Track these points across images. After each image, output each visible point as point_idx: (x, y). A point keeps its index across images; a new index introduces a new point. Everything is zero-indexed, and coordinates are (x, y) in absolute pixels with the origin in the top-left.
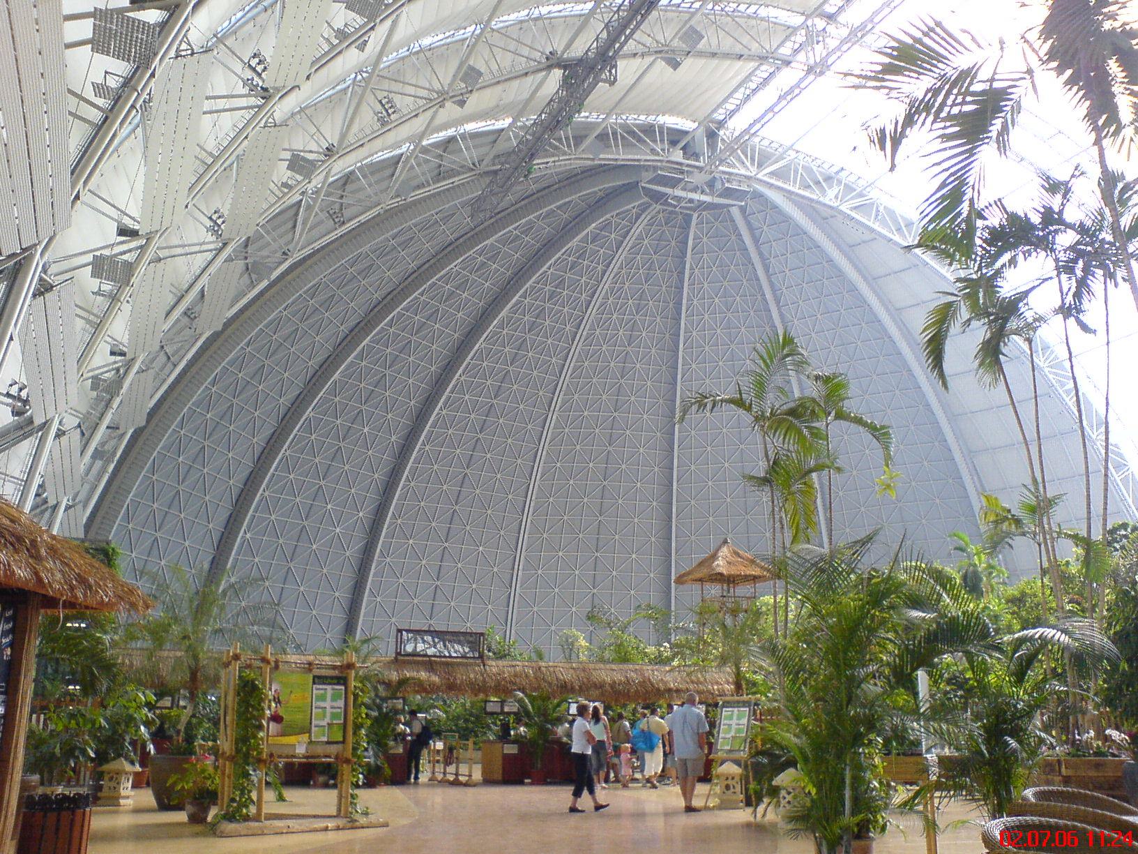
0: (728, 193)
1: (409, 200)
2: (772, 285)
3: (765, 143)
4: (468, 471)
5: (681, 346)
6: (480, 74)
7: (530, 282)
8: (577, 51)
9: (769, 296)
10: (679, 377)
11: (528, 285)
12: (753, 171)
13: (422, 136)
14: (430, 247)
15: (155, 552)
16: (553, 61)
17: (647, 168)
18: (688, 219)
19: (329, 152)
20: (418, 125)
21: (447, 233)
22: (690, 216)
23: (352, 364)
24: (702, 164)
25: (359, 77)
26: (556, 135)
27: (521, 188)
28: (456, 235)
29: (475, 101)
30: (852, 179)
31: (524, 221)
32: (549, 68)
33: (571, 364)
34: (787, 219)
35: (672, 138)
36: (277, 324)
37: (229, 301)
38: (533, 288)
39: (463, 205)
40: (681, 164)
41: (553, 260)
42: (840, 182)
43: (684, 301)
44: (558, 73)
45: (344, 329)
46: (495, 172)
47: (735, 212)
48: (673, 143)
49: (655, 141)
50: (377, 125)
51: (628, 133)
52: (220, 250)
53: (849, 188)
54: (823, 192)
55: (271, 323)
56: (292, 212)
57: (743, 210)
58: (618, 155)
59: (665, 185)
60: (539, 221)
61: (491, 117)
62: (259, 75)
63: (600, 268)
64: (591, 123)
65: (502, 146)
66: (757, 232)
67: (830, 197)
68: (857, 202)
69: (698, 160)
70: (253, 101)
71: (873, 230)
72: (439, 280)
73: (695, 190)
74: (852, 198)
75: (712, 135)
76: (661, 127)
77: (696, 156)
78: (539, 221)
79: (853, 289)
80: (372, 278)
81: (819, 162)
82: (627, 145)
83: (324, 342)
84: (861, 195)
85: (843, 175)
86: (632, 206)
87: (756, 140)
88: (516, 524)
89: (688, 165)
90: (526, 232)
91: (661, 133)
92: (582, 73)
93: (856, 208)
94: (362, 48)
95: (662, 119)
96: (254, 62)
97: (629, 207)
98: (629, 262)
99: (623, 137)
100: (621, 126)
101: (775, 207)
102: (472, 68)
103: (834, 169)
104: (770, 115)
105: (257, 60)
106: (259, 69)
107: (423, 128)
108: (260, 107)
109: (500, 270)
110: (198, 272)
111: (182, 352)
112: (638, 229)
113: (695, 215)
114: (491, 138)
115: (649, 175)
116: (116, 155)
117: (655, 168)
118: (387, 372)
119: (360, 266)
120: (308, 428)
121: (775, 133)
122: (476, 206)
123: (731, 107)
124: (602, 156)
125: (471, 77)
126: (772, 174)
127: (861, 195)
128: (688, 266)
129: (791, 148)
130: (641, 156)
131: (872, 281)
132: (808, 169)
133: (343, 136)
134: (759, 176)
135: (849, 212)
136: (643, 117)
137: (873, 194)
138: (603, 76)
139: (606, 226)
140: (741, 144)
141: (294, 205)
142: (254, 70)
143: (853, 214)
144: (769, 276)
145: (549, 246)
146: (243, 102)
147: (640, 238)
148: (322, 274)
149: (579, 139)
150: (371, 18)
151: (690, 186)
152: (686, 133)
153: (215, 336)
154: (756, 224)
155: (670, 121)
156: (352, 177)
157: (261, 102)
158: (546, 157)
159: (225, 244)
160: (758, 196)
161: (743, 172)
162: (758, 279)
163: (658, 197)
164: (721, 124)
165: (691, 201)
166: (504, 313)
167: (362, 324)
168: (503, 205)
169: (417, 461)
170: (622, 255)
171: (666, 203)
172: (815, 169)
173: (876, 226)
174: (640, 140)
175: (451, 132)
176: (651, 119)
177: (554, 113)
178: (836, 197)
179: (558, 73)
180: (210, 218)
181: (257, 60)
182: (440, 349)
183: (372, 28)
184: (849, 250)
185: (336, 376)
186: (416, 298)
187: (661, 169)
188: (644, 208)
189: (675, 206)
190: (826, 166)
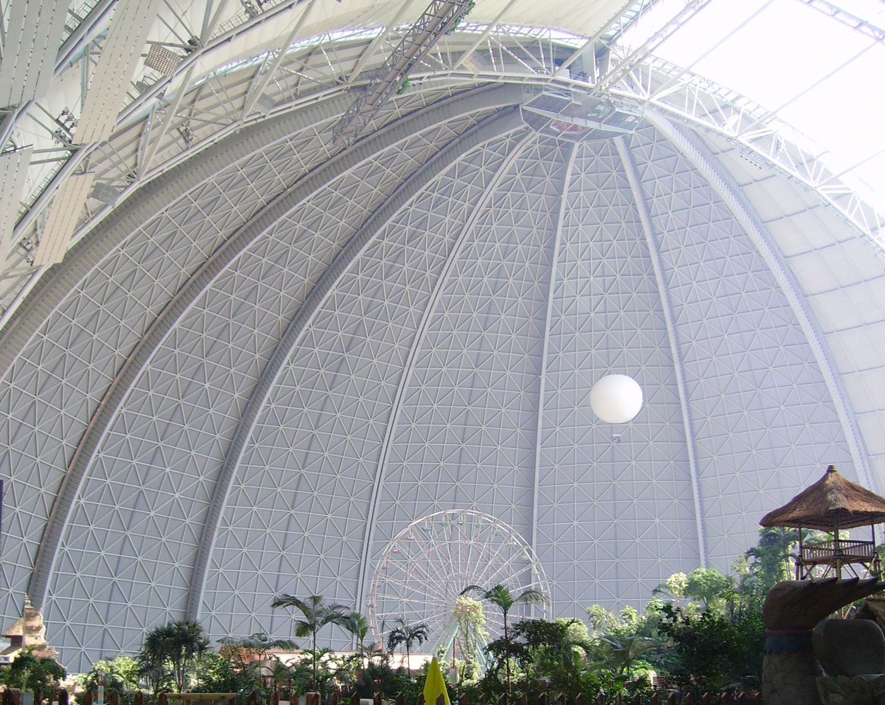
2: (652, 228)
3: (658, 64)
5: (551, 294)
7: (389, 221)
9: (649, 240)
10: (548, 329)
11: (386, 225)
12: (644, 96)
14: (280, 179)
15: (92, 324)
17: (528, 88)
18: (567, 148)
19: (193, 46)
22: (569, 146)
23: (193, 312)
24: (589, 85)
26: (432, 50)
27: (395, 106)
28: (310, 166)
30: (751, 107)
33: (430, 314)
34: (675, 152)
35: (559, 57)
37: (75, 221)
40: (567, 84)
41: (414, 197)
42: (737, 111)
43: (557, 244)
45: (185, 271)
46: (364, 88)
47: (618, 140)
48: (559, 62)
49: (539, 59)
50: (245, 18)
51: (512, 49)
52: (69, 159)
53: (747, 119)
54: (720, 121)
57: (627, 140)
58: (501, 73)
59: (548, 109)
60: (403, 152)
62: (68, 130)
65: (373, 60)
66: (640, 168)
67: (730, 126)
71: (773, 166)
75: (601, 53)
76: (546, 45)
77: (583, 76)
78: (403, 152)
79: (742, 234)
81: (716, 87)
82: (508, 60)
85: (740, 104)
86: (504, 135)
87: (648, 60)
89: (576, 86)
91: (546, 51)
93: (754, 140)
95: (545, 35)
96: (62, 119)
97: (502, 135)
98: (499, 199)
99: (505, 55)
101: (663, 139)
103: (731, 97)
104: (672, 28)
105: (65, 117)
106: (68, 125)
109: (355, 208)
111: (18, 289)
112: (512, 160)
113: (577, 145)
114: (357, 51)
117: (538, 89)
118: (231, 321)
121: (672, 54)
122: (338, 129)
123: (624, 20)
127: (758, 127)
128: (563, 205)
129: (687, 71)
131: (761, 224)
132: (704, 96)
133: (206, 30)
134: (653, 100)
135: (748, 144)
136: (525, 31)
137: (772, 127)
140: (633, 67)
142: (63, 125)
143: (753, 147)
145: (411, 181)
146: (54, 155)
147: (512, 172)
148: (163, 208)
152: (572, 51)
153: (55, 270)
154: (639, 158)
155: (557, 37)
158: (420, 71)
159: (74, 152)
160: (646, 126)
161: (632, 94)
162: (638, 221)
163: (536, 122)
164: (611, 40)
165: (575, 128)
166: (359, 256)
168: (367, 130)
170: (492, 191)
171: (548, 131)
172: (713, 97)
173: (776, 161)
174: (526, 59)
175: (314, 41)
176: (535, 33)
177: (440, 14)
178: (735, 128)
180: (57, 121)
181: (65, 117)
182: (288, 297)
184: (738, 189)
185: (176, 325)
187: (546, 90)
188: (518, 138)
190: (723, 92)
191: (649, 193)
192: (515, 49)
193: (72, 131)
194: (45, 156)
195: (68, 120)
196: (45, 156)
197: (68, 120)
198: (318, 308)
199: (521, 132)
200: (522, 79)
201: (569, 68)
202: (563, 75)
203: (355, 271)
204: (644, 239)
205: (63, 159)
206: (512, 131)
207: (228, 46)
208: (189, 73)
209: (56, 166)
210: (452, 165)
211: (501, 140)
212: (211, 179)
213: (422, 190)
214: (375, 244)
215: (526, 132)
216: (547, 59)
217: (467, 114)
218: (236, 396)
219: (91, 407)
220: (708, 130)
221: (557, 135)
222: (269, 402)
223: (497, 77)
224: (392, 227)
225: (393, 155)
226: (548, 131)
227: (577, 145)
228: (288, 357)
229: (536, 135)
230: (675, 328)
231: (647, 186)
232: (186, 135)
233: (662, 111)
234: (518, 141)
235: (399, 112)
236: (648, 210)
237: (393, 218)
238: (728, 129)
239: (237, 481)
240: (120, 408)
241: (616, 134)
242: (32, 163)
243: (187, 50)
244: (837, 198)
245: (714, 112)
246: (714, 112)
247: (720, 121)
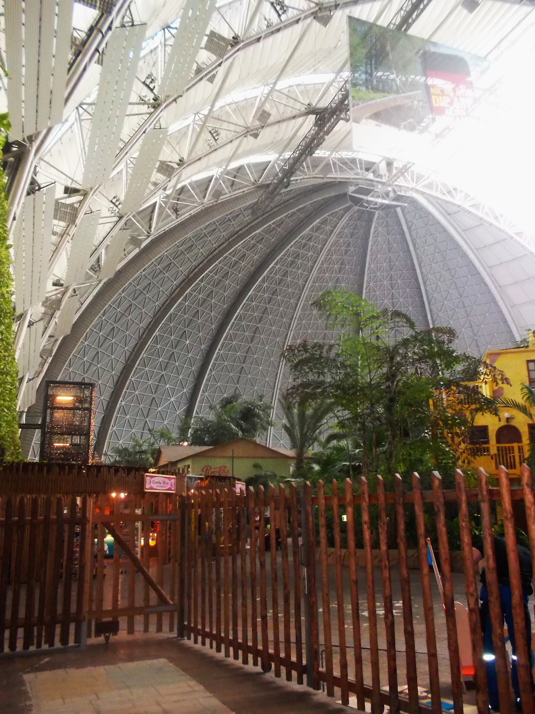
0: (398, 198)
1: (219, 202)
4: (244, 365)
6: (269, 115)
8: (324, 104)
11: (278, 258)
13: (230, 160)
16: (311, 111)
20: (228, 150)
21: (235, 225)
25: (197, 118)
29: (266, 135)
31: (279, 218)
32: (307, 113)
36: (139, 281)
38: (191, 294)
39: (246, 209)
44: (312, 118)
47: (399, 210)
48: (367, 170)
55: (135, 279)
56: (150, 210)
57: (403, 209)
58: (335, 175)
61: (265, 155)
62: (117, 206)
63: (320, 246)
64: (320, 157)
66: (410, 224)
67: (458, 200)
68: (472, 203)
69: (382, 178)
70: (144, 109)
72: (229, 254)
73: (378, 197)
74: (470, 200)
76: (360, 161)
80: (192, 253)
82: (341, 170)
83: (166, 290)
84: (473, 199)
86: (338, 209)
88: (270, 394)
90: (279, 226)
92: (325, 118)
93: (471, 206)
94: (211, 80)
96: (114, 201)
99: (340, 167)
100: (339, 159)
102: (264, 112)
105: (150, 80)
106: (117, 203)
107: (231, 155)
108: (151, 114)
110: (101, 239)
113: (377, 212)
115: (352, 189)
116: (59, 142)
119: (185, 246)
120: (156, 342)
122: (254, 209)
124: (328, 176)
125: (263, 116)
126: (424, 186)
130: (349, 175)
134: (419, 188)
138: (342, 116)
139: (324, 222)
141: (151, 205)
142: (114, 204)
143: (471, 209)
144: (415, 250)
145: (291, 234)
146: (109, 220)
147: (344, 228)
148: (165, 250)
149: (315, 167)
150: (221, 56)
151: (376, 194)
154: (409, 219)
156: (185, 189)
157: (152, 110)
160: (413, 202)
163: (357, 201)
165: (376, 204)
167: (186, 281)
169: (216, 360)
171: (362, 206)
179: (312, 118)
180: (111, 201)
183: (220, 65)
186: (216, 265)
189: (367, 207)
191: (414, 236)
192: (345, 163)
193: (120, 206)
194: (105, 220)
195: (117, 201)
196: (105, 220)
197: (117, 201)
198: (244, 301)
199: (347, 207)
200: (349, 179)
201: (373, 172)
202: (370, 176)
203: (263, 281)
204: (412, 260)
205: (148, 113)
206: (342, 207)
207: (199, 163)
208: (180, 177)
209: (111, 225)
210: (312, 225)
211: (337, 212)
212: (190, 235)
213: (297, 239)
214: (273, 267)
215: (349, 208)
216: (361, 168)
217: (318, 198)
218: (203, 347)
219: (116, 378)
220: (447, 202)
221: (367, 207)
222: (219, 350)
223: (336, 178)
224: (281, 259)
225: (282, 222)
226: (362, 206)
227: (377, 212)
228: (229, 327)
229: (356, 208)
230: (430, 306)
231: (414, 233)
232: (176, 211)
233: (423, 194)
234: (346, 212)
235: (285, 198)
236: (414, 246)
237: (282, 253)
238: (457, 202)
239: (203, 391)
240: (143, 355)
241: (398, 206)
242: (130, 104)
243: (178, 164)
244: (517, 234)
245: (449, 192)
246: (449, 192)
247: (452, 196)
